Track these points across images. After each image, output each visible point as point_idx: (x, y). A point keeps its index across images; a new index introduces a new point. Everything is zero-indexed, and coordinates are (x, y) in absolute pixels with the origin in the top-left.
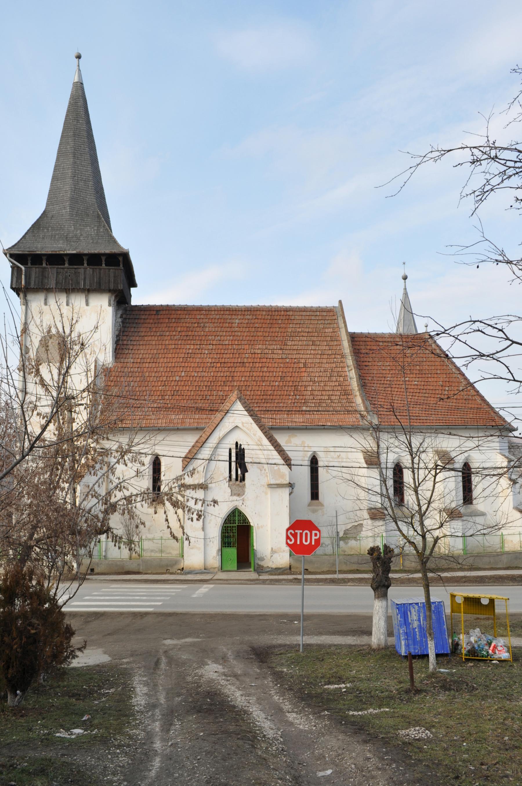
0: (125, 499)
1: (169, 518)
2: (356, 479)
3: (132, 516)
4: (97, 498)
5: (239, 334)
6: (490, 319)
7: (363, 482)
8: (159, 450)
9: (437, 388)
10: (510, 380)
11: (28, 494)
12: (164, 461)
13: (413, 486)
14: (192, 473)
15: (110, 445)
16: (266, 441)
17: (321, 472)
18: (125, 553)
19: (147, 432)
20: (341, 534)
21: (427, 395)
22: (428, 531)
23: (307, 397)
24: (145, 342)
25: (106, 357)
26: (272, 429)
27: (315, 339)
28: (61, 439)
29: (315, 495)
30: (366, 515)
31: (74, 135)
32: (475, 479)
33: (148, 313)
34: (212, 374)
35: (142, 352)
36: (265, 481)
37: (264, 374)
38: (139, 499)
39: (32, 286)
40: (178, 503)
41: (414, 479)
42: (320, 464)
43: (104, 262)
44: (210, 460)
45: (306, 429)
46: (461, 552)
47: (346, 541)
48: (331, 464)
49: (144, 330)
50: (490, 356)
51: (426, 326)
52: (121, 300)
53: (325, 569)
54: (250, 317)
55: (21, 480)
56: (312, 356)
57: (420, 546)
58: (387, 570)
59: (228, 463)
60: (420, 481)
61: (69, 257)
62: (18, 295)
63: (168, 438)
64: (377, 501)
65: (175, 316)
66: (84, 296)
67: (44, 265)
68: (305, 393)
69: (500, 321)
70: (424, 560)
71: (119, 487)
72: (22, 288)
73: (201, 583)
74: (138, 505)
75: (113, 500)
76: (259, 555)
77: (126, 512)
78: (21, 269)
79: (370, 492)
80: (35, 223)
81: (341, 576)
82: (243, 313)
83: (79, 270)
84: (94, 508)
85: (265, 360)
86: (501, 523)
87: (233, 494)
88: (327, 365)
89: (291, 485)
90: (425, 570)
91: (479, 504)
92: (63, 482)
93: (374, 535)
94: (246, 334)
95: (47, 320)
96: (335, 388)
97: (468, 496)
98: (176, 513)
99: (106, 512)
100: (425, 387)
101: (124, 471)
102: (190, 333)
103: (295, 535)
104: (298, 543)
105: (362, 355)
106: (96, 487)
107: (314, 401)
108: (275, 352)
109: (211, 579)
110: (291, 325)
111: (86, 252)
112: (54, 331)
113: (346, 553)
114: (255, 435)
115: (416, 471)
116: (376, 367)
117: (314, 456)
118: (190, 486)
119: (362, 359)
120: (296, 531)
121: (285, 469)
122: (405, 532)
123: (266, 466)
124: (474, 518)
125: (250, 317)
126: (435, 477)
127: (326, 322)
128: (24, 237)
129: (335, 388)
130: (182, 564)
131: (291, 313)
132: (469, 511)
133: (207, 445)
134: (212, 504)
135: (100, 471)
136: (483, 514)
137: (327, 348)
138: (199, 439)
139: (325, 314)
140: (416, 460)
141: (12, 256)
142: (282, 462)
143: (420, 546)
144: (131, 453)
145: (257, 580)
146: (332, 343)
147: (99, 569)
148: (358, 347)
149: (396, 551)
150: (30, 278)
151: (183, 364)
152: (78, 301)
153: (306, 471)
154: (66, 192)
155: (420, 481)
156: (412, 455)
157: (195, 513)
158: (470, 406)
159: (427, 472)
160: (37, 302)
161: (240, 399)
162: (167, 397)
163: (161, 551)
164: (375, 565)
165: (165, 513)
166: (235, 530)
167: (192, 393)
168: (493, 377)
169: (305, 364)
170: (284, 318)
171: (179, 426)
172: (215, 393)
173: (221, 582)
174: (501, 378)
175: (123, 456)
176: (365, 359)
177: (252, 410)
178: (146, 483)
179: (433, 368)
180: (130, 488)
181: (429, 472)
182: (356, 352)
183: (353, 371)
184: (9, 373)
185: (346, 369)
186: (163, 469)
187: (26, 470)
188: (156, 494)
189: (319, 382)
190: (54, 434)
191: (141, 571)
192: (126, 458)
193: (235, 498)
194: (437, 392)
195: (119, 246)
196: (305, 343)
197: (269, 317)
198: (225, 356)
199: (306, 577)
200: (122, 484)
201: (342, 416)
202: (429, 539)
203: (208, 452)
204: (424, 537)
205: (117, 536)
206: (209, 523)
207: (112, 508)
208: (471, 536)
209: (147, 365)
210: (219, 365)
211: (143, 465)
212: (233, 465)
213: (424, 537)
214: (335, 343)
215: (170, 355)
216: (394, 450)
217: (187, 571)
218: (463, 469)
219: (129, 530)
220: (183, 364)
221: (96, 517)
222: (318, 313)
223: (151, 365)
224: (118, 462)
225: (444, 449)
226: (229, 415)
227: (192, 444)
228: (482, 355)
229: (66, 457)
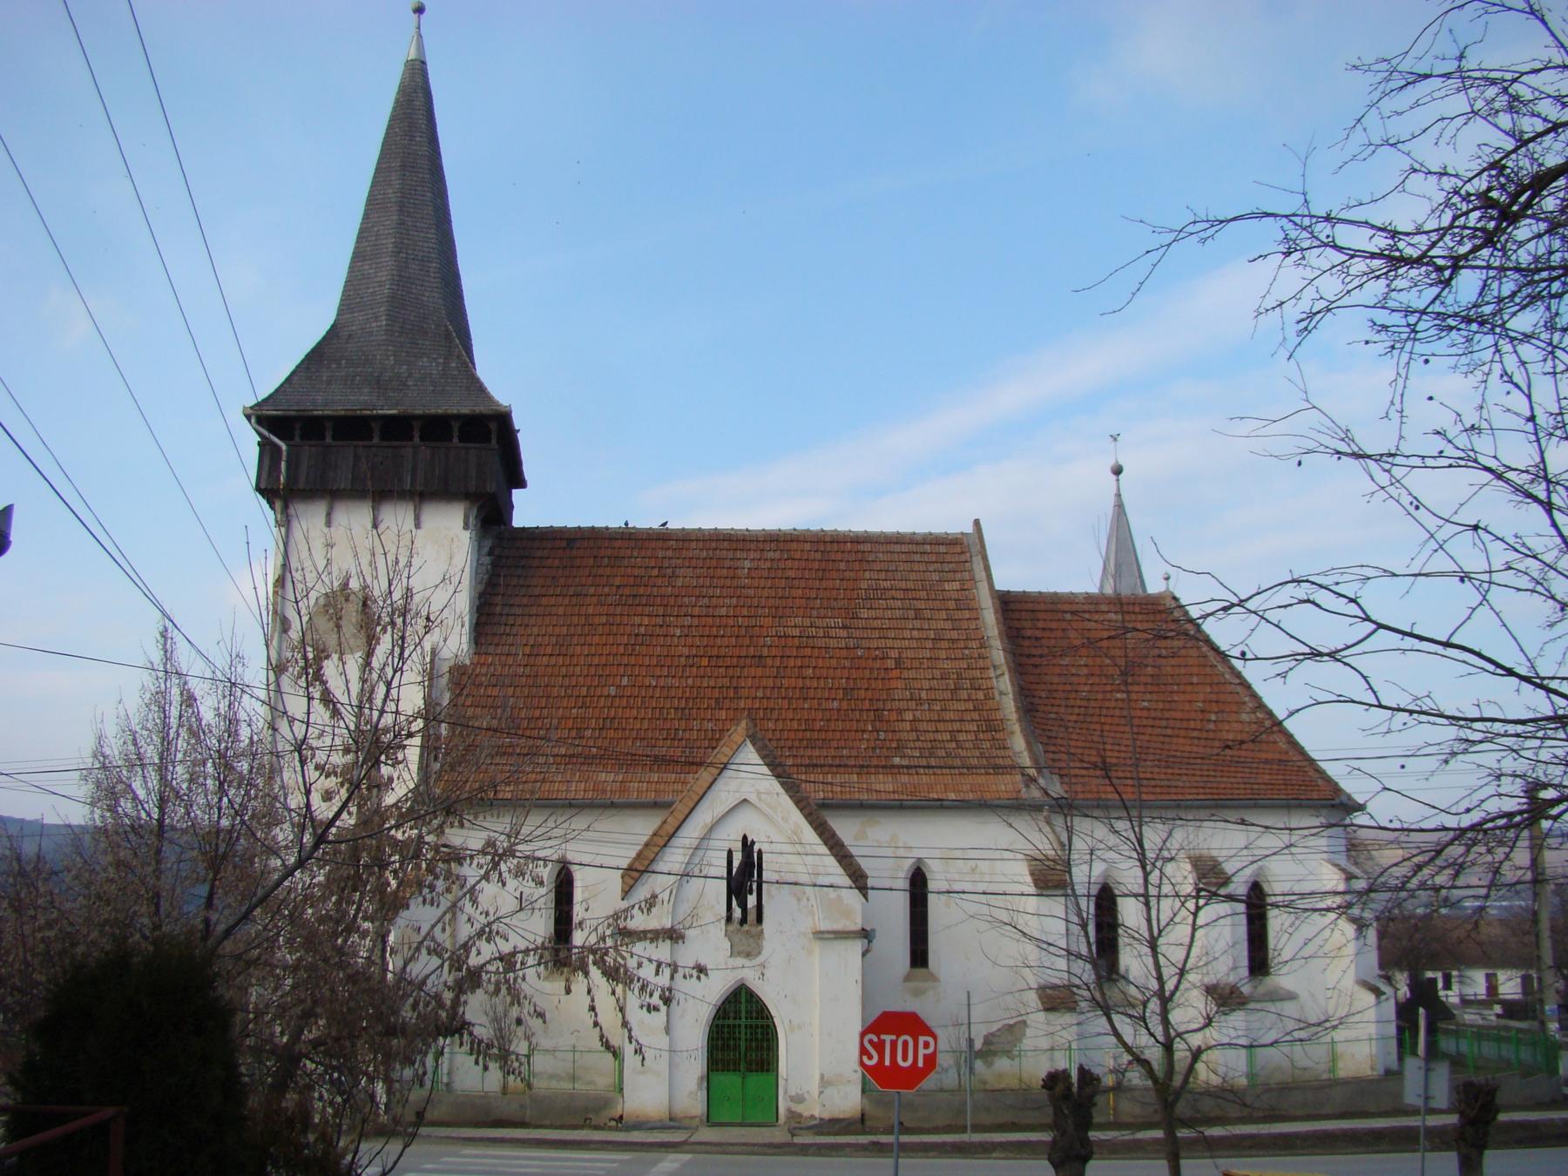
0: (501, 959)
1: (596, 1003)
2: (1021, 920)
3: (516, 997)
4: (440, 955)
5: (751, 592)
6: (1325, 574)
7: (1032, 926)
8: (574, 852)
9: (1193, 715)
12: (581, 878)
13: (1146, 935)
14: (651, 902)
15: (469, 837)
16: (810, 835)
17: (935, 904)
18: (495, 1076)
19: (548, 812)
20: (978, 1045)
21: (1169, 732)
22: (1179, 1035)
23: (904, 736)
24: (541, 610)
25: (455, 642)
26: (824, 806)
28: (364, 822)
29: (919, 955)
30: (1032, 999)
31: (403, 166)
32: (1277, 921)
34: (690, 681)
35: (535, 630)
36: (807, 924)
37: (808, 682)
38: (531, 960)
39: (301, 485)
40: (617, 970)
41: (1149, 920)
42: (932, 886)
43: (456, 434)
44: (686, 875)
46: (1243, 1081)
48: (957, 887)
50: (1332, 655)
51: (1167, 579)
52: (491, 516)
56: (914, 644)
58: (1085, 1122)
60: (1163, 923)
61: (381, 419)
62: (272, 507)
63: (596, 826)
64: (1058, 969)
66: (411, 508)
67: (328, 440)
69: (1346, 577)
70: (1170, 1099)
71: (486, 933)
72: (282, 487)
74: (530, 973)
75: (474, 961)
78: (279, 448)
79: (1052, 949)
80: (313, 351)
81: (977, 1137)
82: (761, 546)
84: (433, 977)
85: (808, 652)
86: (1338, 1015)
88: (947, 665)
89: (866, 934)
90: (1171, 1122)
91: (1282, 978)
92: (365, 919)
93: (1049, 1046)
95: (344, 561)
97: (1259, 961)
98: (613, 993)
100: (1167, 715)
101: (497, 897)
102: (641, 591)
103: (879, 1046)
104: (887, 1063)
105: (1026, 643)
107: (918, 744)
109: (685, 1143)
110: (867, 575)
111: (418, 412)
112: (354, 584)
113: (988, 1087)
115: (1153, 902)
116: (1057, 670)
118: (645, 932)
120: (883, 1037)
121: (852, 897)
122: (1129, 1039)
123: (808, 889)
124: (1279, 1004)
126: (1195, 915)
127: (946, 567)
128: (288, 380)
131: (867, 547)
132: (1261, 990)
133: (675, 841)
134: (695, 973)
136: (1291, 997)
137: (948, 625)
138: (660, 828)
139: (942, 549)
140: (1154, 877)
142: (847, 881)
144: (514, 857)
145: (789, 1145)
146: (958, 615)
148: (1016, 624)
149: (1109, 1080)
151: (625, 660)
152: (397, 517)
153: (899, 904)
155: (1163, 923)
156: (1143, 867)
157: (657, 995)
158: (1264, 756)
159: (1178, 904)
160: (310, 519)
161: (754, 739)
162: (588, 733)
163: (573, 1078)
164: (1058, 1112)
165: (589, 992)
169: (898, 661)
173: (708, 1148)
175: (498, 864)
176: (1034, 651)
177: (780, 765)
178: (540, 926)
179: (1183, 671)
180: (512, 936)
181: (1183, 904)
183: (1007, 677)
185: (992, 673)
186: (578, 895)
188: (560, 950)
189: (931, 701)
192: (503, 867)
193: (740, 961)
194: (1192, 724)
196: (898, 613)
197: (818, 556)
198: (719, 641)
199: (905, 1138)
200: (494, 927)
201: (982, 779)
202: (1181, 1053)
203: (680, 858)
204: (1168, 1047)
205: (481, 1041)
207: (473, 979)
208: (1271, 1045)
210: (705, 662)
211: (542, 883)
213: (1168, 1047)
214: (967, 614)
215: (596, 639)
216: (1101, 852)
218: (1249, 896)
219: (501, 1030)
220: (625, 660)
221: (438, 997)
222: (928, 548)
223: (553, 660)
224: (486, 877)
225: (1214, 853)
226: (727, 773)
227: (645, 839)
228: (1315, 654)
229: (367, 862)
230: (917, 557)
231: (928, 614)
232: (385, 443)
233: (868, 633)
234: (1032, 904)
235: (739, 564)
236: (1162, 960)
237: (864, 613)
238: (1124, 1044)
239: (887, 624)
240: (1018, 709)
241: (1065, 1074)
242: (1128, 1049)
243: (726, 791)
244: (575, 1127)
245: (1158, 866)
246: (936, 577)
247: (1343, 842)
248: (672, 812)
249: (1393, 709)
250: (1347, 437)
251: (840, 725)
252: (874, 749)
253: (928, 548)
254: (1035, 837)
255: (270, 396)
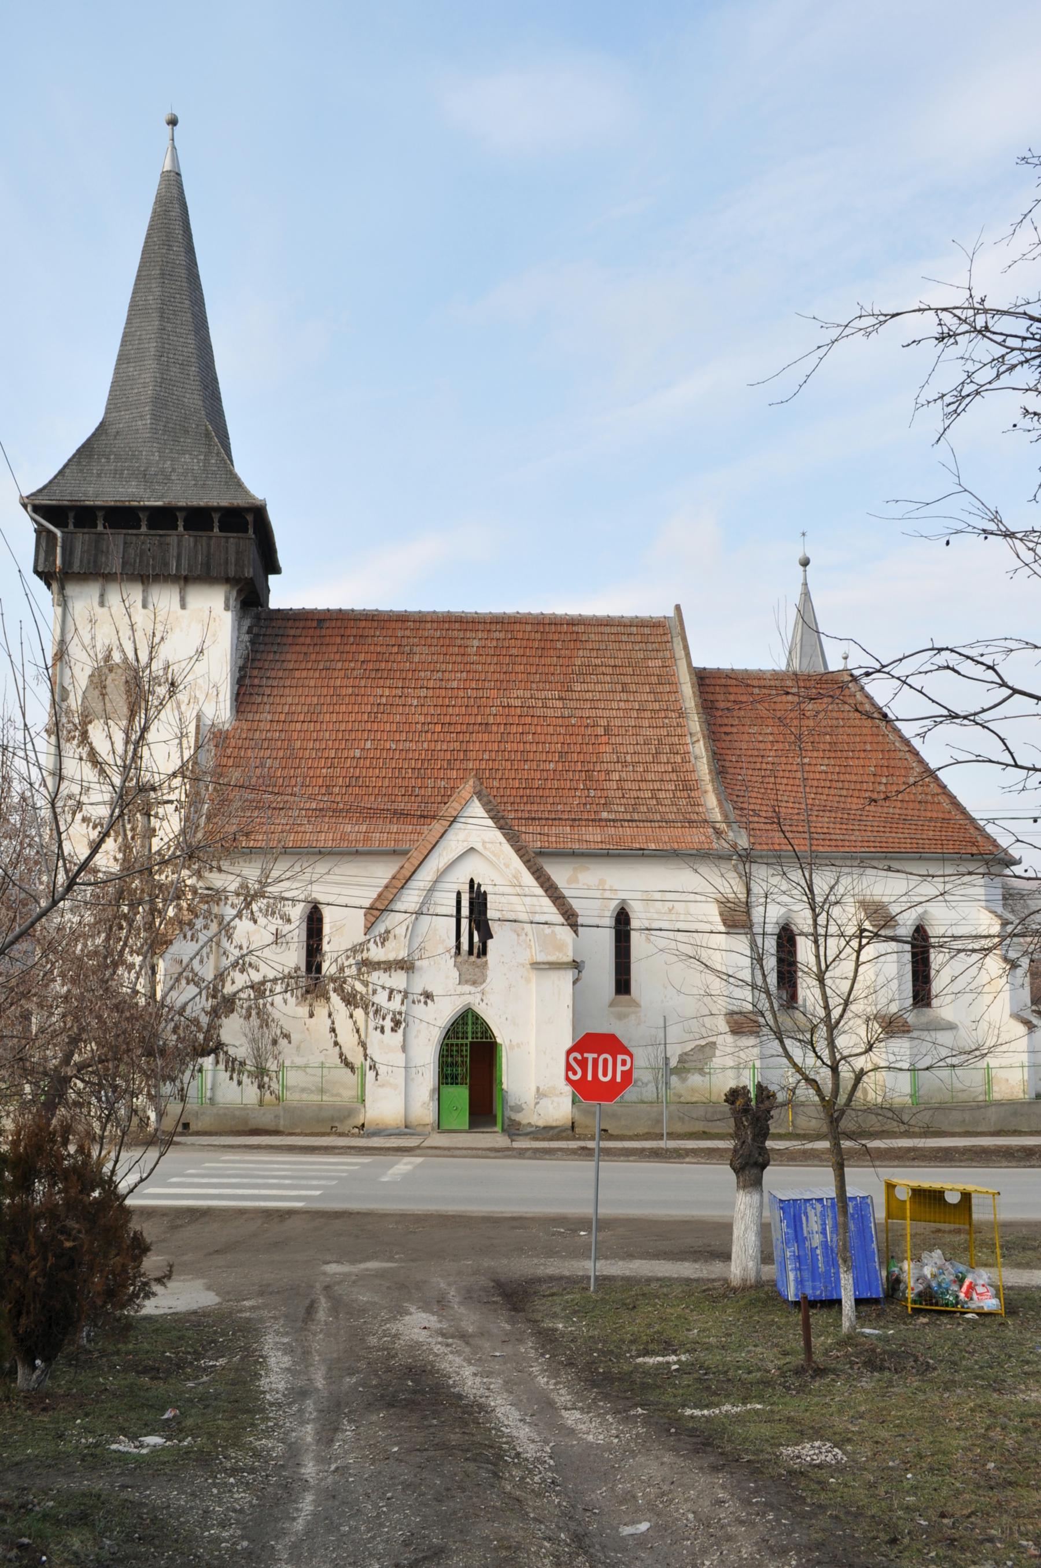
0: (252, 987)
1: (336, 1026)
2: (704, 955)
3: (265, 1019)
4: (197, 984)
5: (479, 668)
6: (970, 646)
7: (717, 960)
8: (319, 893)
9: (865, 778)
10: (1007, 765)
11: (63, 975)
12: (327, 913)
13: (815, 969)
15: (225, 881)
16: (528, 879)
17: (637, 940)
20: (673, 1063)
21: (844, 793)
22: (844, 1058)
23: (611, 793)
24: (294, 682)
26: (541, 854)
27: (627, 679)
29: (623, 985)
30: (722, 1025)
31: (162, 275)
33: (301, 624)
34: (425, 745)
35: (289, 700)
36: (526, 956)
38: (278, 988)
39: (76, 568)
40: (355, 996)
41: (817, 956)
42: (634, 923)
43: (216, 524)
44: (419, 913)
45: (608, 855)
47: (684, 1075)
49: (294, 657)
51: (846, 658)
52: (250, 599)
53: (641, 1130)
54: (502, 635)
55: (50, 947)
57: (827, 1087)
59: (454, 919)
60: (830, 959)
61: (151, 514)
62: (49, 586)
63: (336, 870)
64: (745, 998)
65: (354, 632)
66: (178, 590)
67: (100, 528)
68: (607, 785)
69: (990, 649)
70: (836, 1115)
72: (56, 573)
73: (399, 1153)
74: (278, 999)
75: (229, 989)
76: (511, 1103)
77: (254, 1012)
78: (55, 535)
79: (731, 980)
80: (83, 446)
81: (672, 1144)
82: (488, 627)
83: (168, 539)
85: (528, 720)
86: (987, 1045)
87: (463, 980)
88: (649, 732)
89: (576, 965)
90: (835, 1134)
91: (944, 1008)
93: (737, 1065)
94: (492, 668)
96: (666, 777)
98: (351, 1016)
99: (214, 1013)
103: (583, 1064)
104: (590, 1078)
105: (720, 713)
106: (196, 963)
107: (623, 801)
108: (550, 703)
109: (418, 1147)
110: (581, 653)
113: (682, 1100)
114: (507, 866)
115: (821, 940)
116: (746, 737)
117: (623, 909)
118: (379, 963)
119: (719, 721)
120: (586, 1055)
121: (565, 933)
122: (798, 1060)
123: (528, 926)
124: (933, 1033)
125: (502, 635)
126: (858, 952)
127: (650, 647)
128: (61, 472)
129: (666, 777)
130: (362, 1117)
131: (581, 629)
132: (924, 1019)
133: (412, 884)
135: (205, 932)
136: (951, 1027)
137: (651, 697)
138: (398, 872)
139: (647, 631)
140: (822, 919)
141: (37, 509)
142: (560, 919)
143: (827, 1087)
144: (264, 897)
145: (508, 1149)
147: (200, 1124)
148: (710, 697)
149: (781, 1097)
150: (71, 553)
151: (369, 726)
153: (606, 939)
154: (145, 385)
155: (830, 959)
156: (813, 910)
157: (389, 1018)
158: (929, 814)
159: (843, 943)
160: (84, 600)
161: (479, 795)
162: (336, 790)
163: (322, 1091)
165: (330, 1015)
166: (466, 1052)
167: (386, 782)
168: (975, 758)
169: (607, 728)
170: (568, 637)
171: (360, 847)
172: (430, 783)
174: (991, 761)
175: (250, 904)
176: (726, 721)
177: (503, 818)
178: (293, 957)
179: (858, 739)
181: (848, 943)
182: (708, 707)
183: (701, 743)
184: (28, 739)
185: (688, 740)
186: (327, 929)
187: (60, 929)
188: (313, 978)
189: (634, 764)
190: (116, 859)
191: (281, 1129)
192: (254, 907)
193: (467, 988)
195: (246, 492)
196: (607, 687)
197: (538, 636)
199: (605, 1144)
200: (247, 959)
203: (416, 899)
204: (834, 1069)
205: (234, 1060)
206: (417, 1036)
207: (227, 1005)
208: (927, 1069)
209: (298, 726)
210: (438, 728)
211: (289, 921)
212: (465, 923)
213: (834, 1069)
214: (667, 688)
215: (343, 708)
216: (780, 899)
217: (371, 1130)
218: (913, 938)
219: (258, 1049)
220: (369, 726)
221: (196, 1022)
222: (634, 630)
224: (239, 915)
225: (877, 898)
226: (456, 825)
227: (385, 882)
229: (139, 905)
230: (624, 638)
231: (633, 687)
232: (153, 532)
233: (581, 704)
234: (721, 940)
235: (468, 643)
236: (829, 991)
237: (577, 687)
238: (795, 1065)
239: (598, 696)
240: (710, 771)
241: (745, 1090)
242: (798, 1069)
243: (456, 841)
244: (323, 1134)
245: (847, 911)
246: (641, 655)
247: (1000, 891)
248: (408, 859)
249: (1029, 769)
250: (996, 518)
251: (556, 784)
252: (585, 804)
253: (634, 630)
254: (727, 883)
255: (45, 488)
